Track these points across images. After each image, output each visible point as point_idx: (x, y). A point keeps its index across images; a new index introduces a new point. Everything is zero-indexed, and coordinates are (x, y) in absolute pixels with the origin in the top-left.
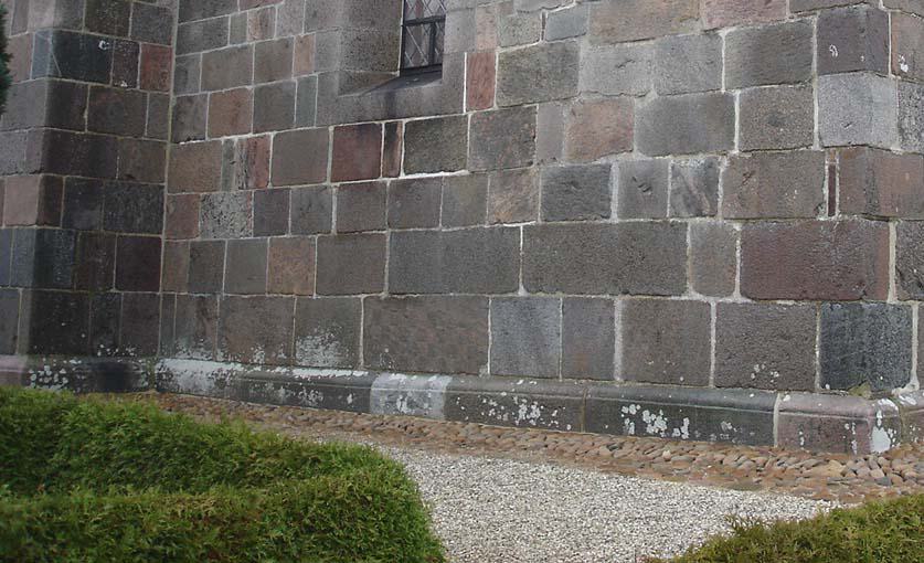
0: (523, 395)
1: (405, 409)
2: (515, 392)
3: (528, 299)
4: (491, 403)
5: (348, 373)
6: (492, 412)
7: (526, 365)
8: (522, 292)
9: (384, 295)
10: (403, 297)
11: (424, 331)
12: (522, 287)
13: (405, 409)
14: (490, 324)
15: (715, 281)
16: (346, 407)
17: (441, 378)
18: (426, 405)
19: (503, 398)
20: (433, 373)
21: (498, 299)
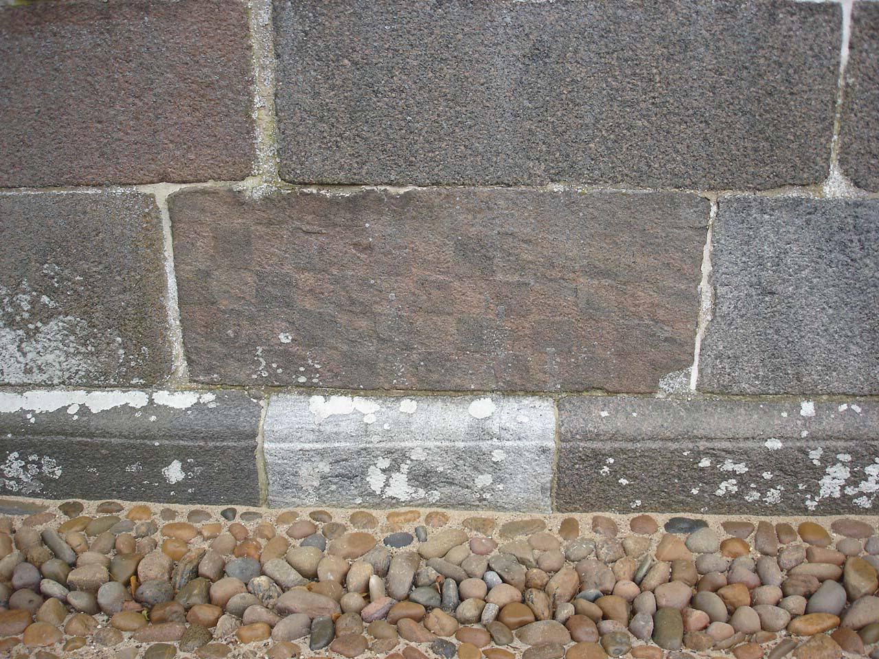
0: (841, 444)
1: (400, 487)
2: (813, 437)
3: (857, 205)
4: (729, 466)
5: (137, 399)
6: (730, 486)
7: (828, 368)
8: (836, 187)
9: (255, 187)
10: (347, 193)
11: (440, 286)
12: (836, 173)
13: (400, 487)
14: (706, 268)
15: (868, 350)
16: (166, 493)
17: (503, 402)
18: (484, 480)
19: (769, 453)
20: (478, 393)
21: (745, 206)
